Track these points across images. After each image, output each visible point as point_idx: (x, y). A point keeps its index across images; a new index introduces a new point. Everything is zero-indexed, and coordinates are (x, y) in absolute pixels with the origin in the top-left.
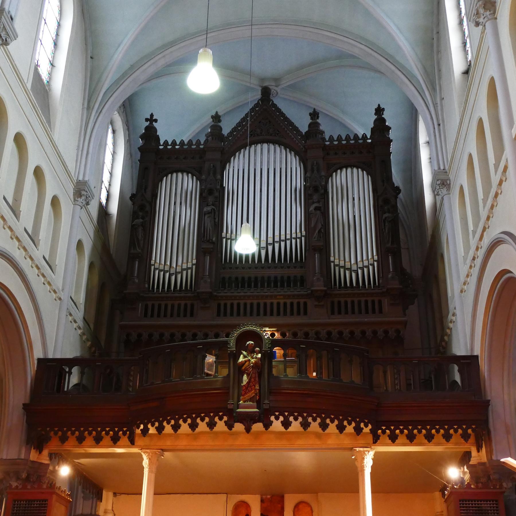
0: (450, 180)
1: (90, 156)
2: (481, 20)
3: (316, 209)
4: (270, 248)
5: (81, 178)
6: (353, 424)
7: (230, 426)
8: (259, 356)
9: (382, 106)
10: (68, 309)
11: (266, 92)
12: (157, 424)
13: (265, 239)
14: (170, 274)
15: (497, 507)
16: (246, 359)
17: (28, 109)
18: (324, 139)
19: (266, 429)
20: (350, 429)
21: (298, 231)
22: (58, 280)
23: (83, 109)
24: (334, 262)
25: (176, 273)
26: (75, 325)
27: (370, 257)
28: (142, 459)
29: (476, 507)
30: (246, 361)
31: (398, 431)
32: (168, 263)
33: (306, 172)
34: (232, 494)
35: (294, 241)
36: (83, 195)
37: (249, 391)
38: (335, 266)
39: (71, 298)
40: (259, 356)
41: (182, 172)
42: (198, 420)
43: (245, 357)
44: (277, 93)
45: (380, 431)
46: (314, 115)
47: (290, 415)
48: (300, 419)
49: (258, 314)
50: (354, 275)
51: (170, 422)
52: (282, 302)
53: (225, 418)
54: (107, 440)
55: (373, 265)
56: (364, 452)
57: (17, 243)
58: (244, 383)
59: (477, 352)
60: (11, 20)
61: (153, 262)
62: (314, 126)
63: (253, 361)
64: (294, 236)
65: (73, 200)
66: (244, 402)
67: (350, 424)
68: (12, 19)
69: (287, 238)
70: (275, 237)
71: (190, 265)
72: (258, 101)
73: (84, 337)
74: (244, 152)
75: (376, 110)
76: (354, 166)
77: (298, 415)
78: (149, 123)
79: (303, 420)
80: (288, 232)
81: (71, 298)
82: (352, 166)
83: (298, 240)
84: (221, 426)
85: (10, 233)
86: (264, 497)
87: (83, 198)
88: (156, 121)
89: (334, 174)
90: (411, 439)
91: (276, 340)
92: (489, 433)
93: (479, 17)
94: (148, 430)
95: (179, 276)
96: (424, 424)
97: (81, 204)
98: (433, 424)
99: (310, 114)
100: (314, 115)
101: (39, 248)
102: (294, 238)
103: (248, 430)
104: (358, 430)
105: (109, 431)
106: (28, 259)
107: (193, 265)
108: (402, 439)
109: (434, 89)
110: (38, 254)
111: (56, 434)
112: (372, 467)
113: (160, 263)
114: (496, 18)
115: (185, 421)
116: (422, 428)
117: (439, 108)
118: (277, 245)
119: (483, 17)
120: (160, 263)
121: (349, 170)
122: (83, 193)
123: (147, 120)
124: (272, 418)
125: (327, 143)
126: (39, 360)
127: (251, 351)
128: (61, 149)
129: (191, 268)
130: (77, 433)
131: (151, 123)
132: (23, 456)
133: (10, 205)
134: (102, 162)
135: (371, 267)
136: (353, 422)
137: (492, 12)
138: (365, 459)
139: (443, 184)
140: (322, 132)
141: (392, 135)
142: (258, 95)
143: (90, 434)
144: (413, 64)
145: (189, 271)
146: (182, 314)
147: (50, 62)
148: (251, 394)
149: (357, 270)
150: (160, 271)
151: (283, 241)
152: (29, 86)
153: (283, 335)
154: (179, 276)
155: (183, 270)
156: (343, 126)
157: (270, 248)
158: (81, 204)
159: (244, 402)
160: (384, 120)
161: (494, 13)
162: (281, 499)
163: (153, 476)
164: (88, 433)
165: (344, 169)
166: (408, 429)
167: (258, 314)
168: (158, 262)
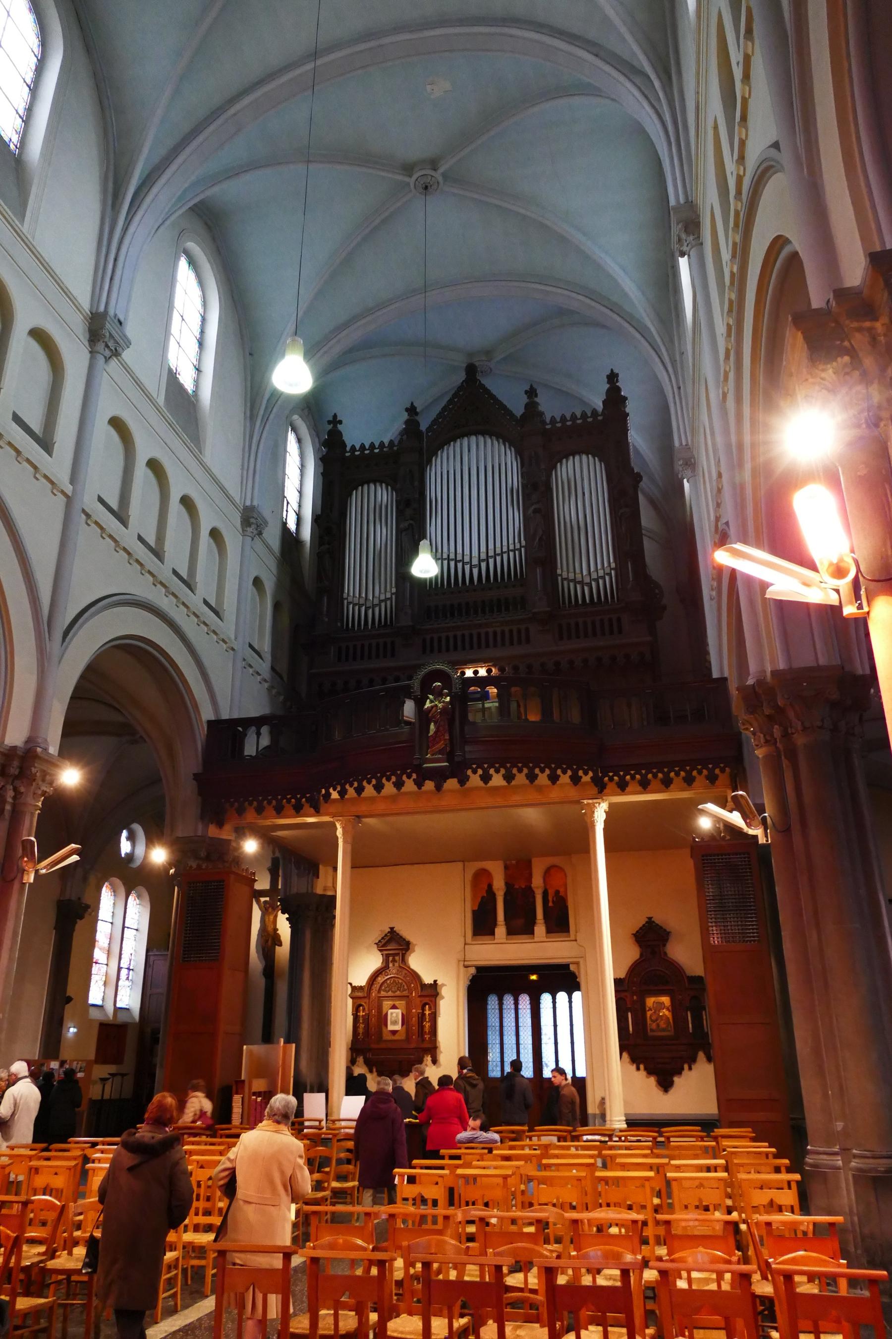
0: (694, 458)
1: (257, 476)
2: (685, 248)
3: (536, 511)
4: (483, 565)
5: (248, 503)
6: (569, 773)
7: (419, 784)
8: (448, 699)
9: (616, 371)
10: (244, 660)
11: (471, 370)
12: (356, 784)
13: (477, 555)
14: (366, 608)
15: (749, 861)
16: (433, 704)
17: (162, 428)
18: (544, 423)
19: (419, 788)
20: (565, 779)
21: (516, 541)
22: (228, 627)
23: (245, 419)
24: (561, 575)
25: (374, 606)
26: (259, 678)
27: (606, 565)
28: (336, 829)
29: (722, 863)
30: (432, 707)
31: (650, 776)
32: (364, 595)
33: (522, 466)
34: (469, 861)
35: (511, 554)
36: (252, 523)
37: (438, 743)
38: (563, 580)
39: (251, 646)
40: (448, 699)
41: (375, 482)
42: (404, 777)
43: (431, 702)
44: (491, 369)
45: (606, 779)
46: (531, 393)
47: (513, 766)
48: (503, 771)
49: (503, 644)
50: (586, 589)
51: (353, 784)
52: (499, 630)
53: (414, 776)
54: (289, 810)
55: (610, 575)
56: (593, 804)
57: (164, 590)
58: (431, 733)
59: (726, 675)
60: (119, 325)
61: (345, 595)
62: (532, 407)
63: (440, 705)
64: (511, 547)
65: (241, 532)
66: (432, 755)
67: (564, 772)
68: (121, 323)
69: (504, 550)
70: (489, 551)
71: (388, 595)
72: (462, 383)
73: (274, 691)
74: (448, 450)
75: (608, 377)
76: (583, 452)
77: (500, 767)
78: (332, 425)
79: (506, 771)
80: (505, 543)
81: (251, 646)
82: (580, 453)
83: (517, 552)
84: (409, 785)
85: (151, 579)
86: (508, 862)
87: (253, 526)
88: (340, 422)
89: (559, 464)
90: (645, 786)
91: (493, 677)
92: (744, 770)
93: (682, 245)
94: (330, 794)
95: (377, 610)
96: (638, 768)
97: (251, 534)
98: (649, 767)
99: (526, 392)
100: (531, 393)
101: (197, 592)
102: (512, 550)
103: (439, 788)
104: (576, 780)
105: (291, 798)
106: (182, 607)
107: (392, 594)
108: (655, 784)
109: (672, 341)
110: (195, 601)
111: (269, 803)
112: (605, 821)
113: (354, 596)
114: (702, 244)
115: (369, 783)
116: (658, 772)
117: (679, 365)
118: (491, 561)
119: (686, 244)
120: (354, 596)
121: (577, 458)
122: (252, 520)
123: (329, 422)
124: (469, 772)
125: (548, 427)
126: (210, 723)
127: (439, 694)
128: (215, 471)
129: (391, 599)
130: (236, 804)
131: (335, 426)
132: (200, 833)
133: (150, 545)
134: (280, 482)
135: (607, 578)
136: (547, 769)
137: (696, 236)
138: (596, 813)
139: (686, 464)
140: (541, 414)
141: (630, 407)
142: (461, 377)
143: (289, 801)
144: (642, 311)
145: (388, 603)
146: (475, 646)
147: (195, 367)
148: (440, 745)
149: (591, 583)
150: (354, 605)
151: (498, 555)
152: (161, 400)
153: (501, 670)
154: (377, 610)
155: (381, 601)
156: (582, 402)
157: (483, 565)
158: (251, 534)
159: (432, 755)
160: (619, 389)
161: (699, 237)
162: (528, 865)
163: (349, 847)
164: (249, 804)
165: (571, 458)
166: (707, 769)
167: (503, 644)
168: (352, 594)
